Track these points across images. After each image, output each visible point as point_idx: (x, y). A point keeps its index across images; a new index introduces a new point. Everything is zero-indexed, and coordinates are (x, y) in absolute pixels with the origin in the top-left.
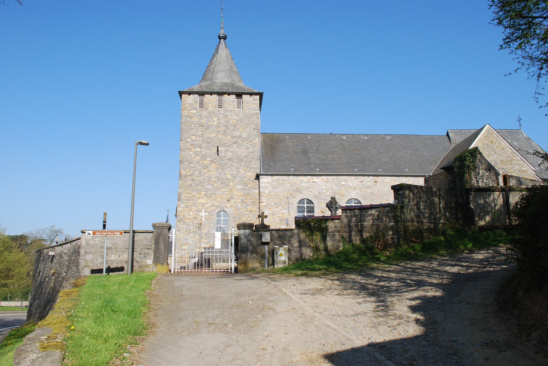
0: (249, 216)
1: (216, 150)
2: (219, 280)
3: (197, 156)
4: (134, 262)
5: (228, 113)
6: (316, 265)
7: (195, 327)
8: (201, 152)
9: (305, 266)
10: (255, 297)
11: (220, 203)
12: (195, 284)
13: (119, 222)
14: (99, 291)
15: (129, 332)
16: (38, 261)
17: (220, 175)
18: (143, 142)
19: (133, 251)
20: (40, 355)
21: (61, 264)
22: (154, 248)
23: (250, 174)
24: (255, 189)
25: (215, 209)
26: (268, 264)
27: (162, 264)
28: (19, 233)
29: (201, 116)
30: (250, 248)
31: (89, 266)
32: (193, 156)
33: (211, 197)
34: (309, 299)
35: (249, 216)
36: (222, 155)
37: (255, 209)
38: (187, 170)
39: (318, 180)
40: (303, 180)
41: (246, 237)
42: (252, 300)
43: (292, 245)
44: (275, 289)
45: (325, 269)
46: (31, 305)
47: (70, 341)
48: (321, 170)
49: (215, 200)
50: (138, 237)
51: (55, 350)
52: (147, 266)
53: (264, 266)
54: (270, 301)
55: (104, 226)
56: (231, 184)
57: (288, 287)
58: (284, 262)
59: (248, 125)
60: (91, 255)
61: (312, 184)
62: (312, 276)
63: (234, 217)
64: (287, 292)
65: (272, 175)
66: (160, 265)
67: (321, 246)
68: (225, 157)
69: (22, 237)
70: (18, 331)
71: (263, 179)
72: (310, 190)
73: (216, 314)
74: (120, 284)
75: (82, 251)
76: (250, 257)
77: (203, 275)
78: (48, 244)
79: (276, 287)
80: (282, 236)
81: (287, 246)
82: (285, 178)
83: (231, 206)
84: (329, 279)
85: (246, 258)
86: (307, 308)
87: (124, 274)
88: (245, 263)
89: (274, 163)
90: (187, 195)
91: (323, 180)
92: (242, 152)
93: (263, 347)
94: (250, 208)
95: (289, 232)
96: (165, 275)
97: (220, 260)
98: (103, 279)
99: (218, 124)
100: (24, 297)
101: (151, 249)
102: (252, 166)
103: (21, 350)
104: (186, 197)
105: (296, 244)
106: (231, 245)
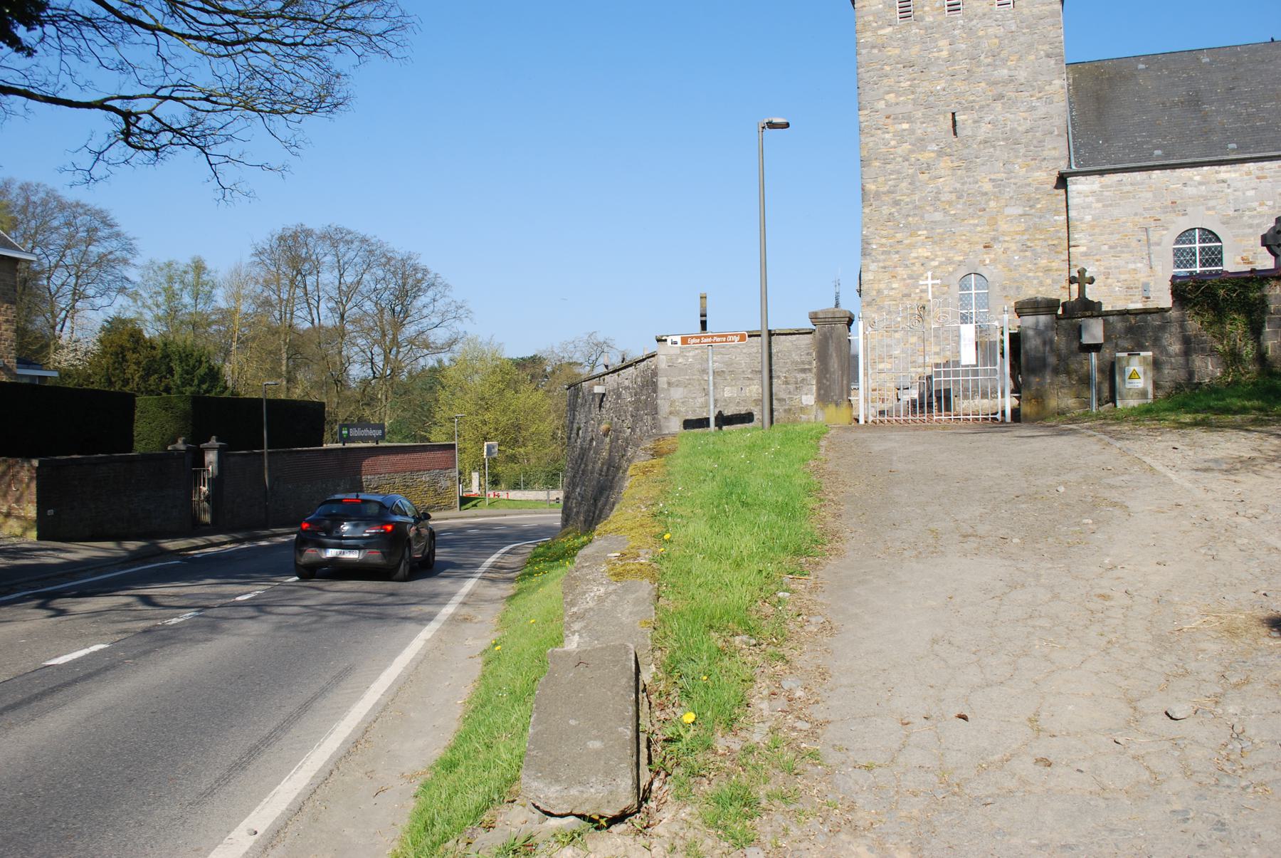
0: (1041, 284)
1: (950, 123)
2: (976, 437)
3: (902, 141)
4: (775, 402)
5: (975, 22)
6: (1234, 400)
7: (931, 541)
8: (912, 132)
9: (1201, 401)
10: (1072, 477)
11: (966, 254)
12: (920, 448)
13: (735, 315)
14: (709, 464)
15: (785, 548)
16: (573, 407)
17: (963, 184)
18: (775, 120)
19: (771, 377)
20: (611, 588)
21: (619, 411)
22: (818, 367)
23: (1041, 175)
24: (1057, 212)
25: (955, 270)
26: (1099, 400)
27: (837, 405)
28: (528, 353)
29: (905, 40)
30: (1052, 360)
31: (677, 413)
32: (893, 143)
33: (942, 240)
34: (1218, 483)
35: (1041, 284)
36: (965, 133)
37: (1059, 263)
38: (881, 179)
39: (1233, 175)
40: (1191, 179)
41: (1038, 332)
42: (1065, 484)
43: (1163, 350)
44: (1125, 459)
45: (1260, 409)
46: (567, 498)
47: (666, 564)
48: (1241, 148)
49: (952, 248)
50: (780, 344)
51: (639, 580)
52: (803, 409)
53: (1088, 404)
54: (1112, 487)
55: (704, 325)
56: (992, 204)
57: (1159, 453)
58: (1143, 394)
59: (1031, 46)
60: (680, 390)
61: (1215, 187)
62: (1220, 427)
63: (1004, 288)
64: (1158, 466)
65: (1101, 173)
66: (832, 409)
67: (1248, 350)
68: (973, 137)
69: (535, 361)
70: (549, 548)
71: (1078, 186)
72: (1211, 203)
73: (977, 513)
74: (751, 448)
75: (662, 381)
76: (1051, 384)
77: (935, 427)
78: (585, 371)
79: (1124, 453)
80: (1136, 327)
81: (1150, 353)
82: (1144, 175)
83: (993, 261)
84: (1270, 434)
85: (1041, 384)
86: (1215, 506)
87: (754, 428)
88: (1040, 398)
89: (1106, 141)
90: (884, 241)
91: (1248, 173)
92: (1018, 119)
93: (1102, 592)
94: (1043, 262)
95: (1154, 316)
96: (846, 429)
97: (975, 392)
98: (712, 439)
99: (951, 55)
100: (551, 482)
101: (810, 370)
102: (1046, 153)
103: (575, 578)
104: (882, 245)
105: (1176, 348)
106: (1002, 354)
